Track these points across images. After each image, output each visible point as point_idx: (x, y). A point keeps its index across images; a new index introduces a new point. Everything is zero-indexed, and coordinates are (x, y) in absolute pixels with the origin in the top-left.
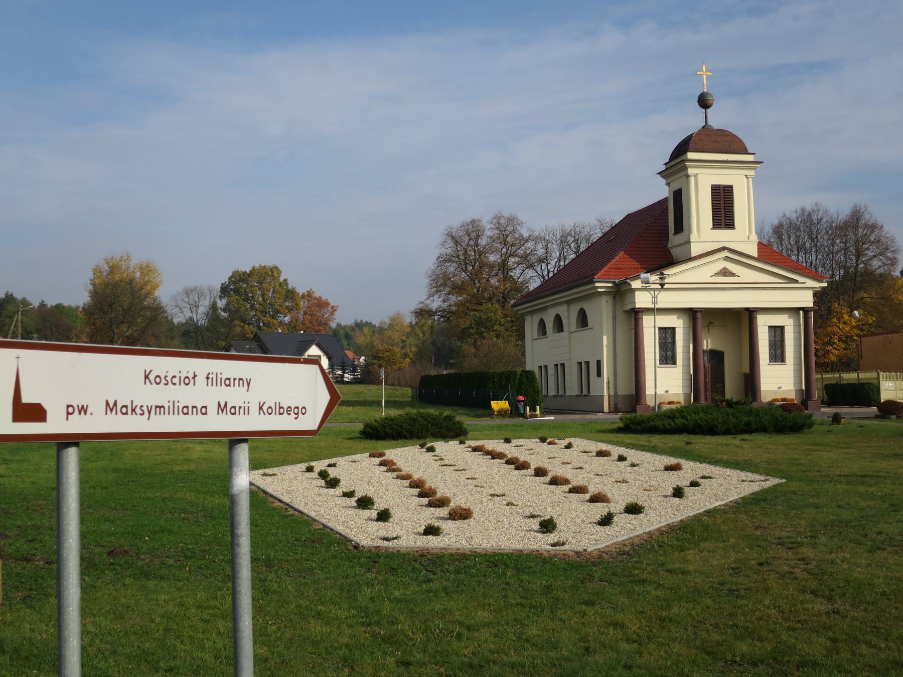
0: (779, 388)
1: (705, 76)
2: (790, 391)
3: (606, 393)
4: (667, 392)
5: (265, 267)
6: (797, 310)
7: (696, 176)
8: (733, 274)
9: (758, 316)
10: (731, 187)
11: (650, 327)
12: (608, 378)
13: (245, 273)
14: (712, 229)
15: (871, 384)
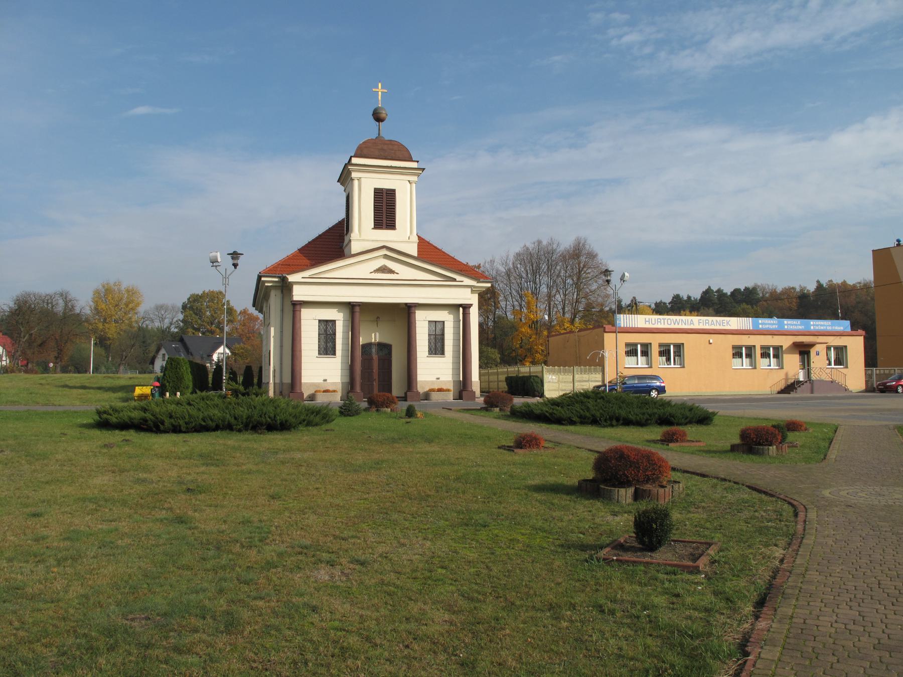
0: (438, 379)
1: (380, 93)
2: (449, 381)
3: (271, 381)
4: (325, 380)
5: (213, 292)
6: (458, 306)
7: (359, 179)
8: (391, 272)
9: (416, 311)
10: (394, 191)
11: (309, 322)
12: (274, 367)
13: (198, 295)
14: (373, 229)
15: (536, 376)
